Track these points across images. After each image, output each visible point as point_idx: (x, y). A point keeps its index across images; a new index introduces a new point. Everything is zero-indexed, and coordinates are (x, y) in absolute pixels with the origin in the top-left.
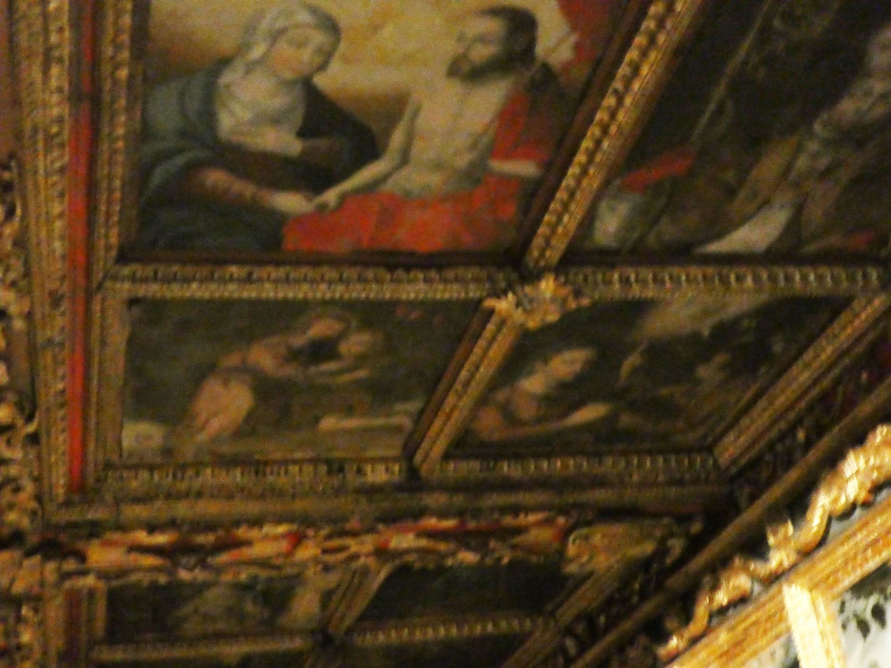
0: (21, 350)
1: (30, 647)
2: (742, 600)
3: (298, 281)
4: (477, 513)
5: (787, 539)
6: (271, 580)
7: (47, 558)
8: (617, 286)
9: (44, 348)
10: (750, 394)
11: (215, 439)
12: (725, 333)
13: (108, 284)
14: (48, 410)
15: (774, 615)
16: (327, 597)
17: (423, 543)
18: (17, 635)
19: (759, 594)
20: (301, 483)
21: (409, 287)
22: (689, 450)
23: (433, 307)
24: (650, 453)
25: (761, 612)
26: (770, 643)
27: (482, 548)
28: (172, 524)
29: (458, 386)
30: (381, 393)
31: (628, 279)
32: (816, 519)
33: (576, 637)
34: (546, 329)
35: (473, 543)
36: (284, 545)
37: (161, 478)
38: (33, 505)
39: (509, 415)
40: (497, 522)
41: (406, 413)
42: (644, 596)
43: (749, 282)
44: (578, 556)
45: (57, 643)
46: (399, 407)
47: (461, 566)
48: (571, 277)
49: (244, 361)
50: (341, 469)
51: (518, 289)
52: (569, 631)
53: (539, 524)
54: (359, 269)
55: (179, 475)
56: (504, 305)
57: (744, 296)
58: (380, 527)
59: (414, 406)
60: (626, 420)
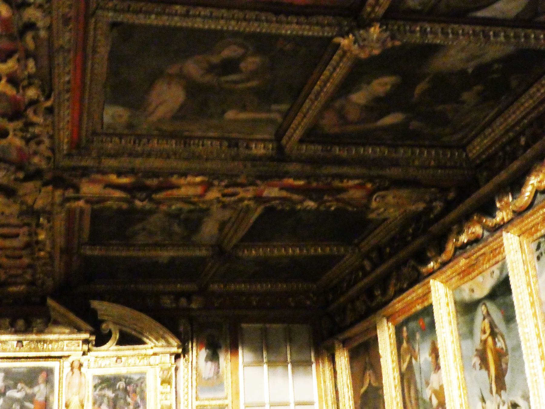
0: (43, 51)
1: (43, 243)
2: (476, 241)
3: (217, 18)
4: (317, 178)
5: (508, 204)
6: (191, 211)
7: (56, 187)
8: (418, 35)
9: (25, 110)
10: (492, 114)
11: (160, 121)
12: (483, 71)
13: (99, 12)
14: (59, 94)
15: (496, 249)
16: (223, 225)
17: (284, 194)
18: (36, 234)
19: (488, 237)
20: (212, 153)
21: (288, 26)
22: (449, 147)
23: (300, 41)
24: (426, 147)
25: (487, 248)
26: (490, 267)
27: (319, 200)
28: (132, 172)
29: (312, 96)
30: (265, 97)
31: (426, 29)
32: (528, 192)
33: (370, 259)
34: (372, 59)
35: (314, 196)
36: (199, 190)
37: (126, 143)
38: (48, 153)
39: (342, 116)
40: (330, 184)
41: (278, 111)
42: (415, 236)
43: (502, 38)
44: (377, 208)
45: (61, 241)
46: (274, 107)
47: (305, 210)
48: (390, 26)
49: (181, 69)
50: (237, 145)
51: (356, 32)
52: (367, 256)
53: (357, 187)
54: (257, 13)
55: (137, 142)
56: (345, 42)
57: (498, 46)
58: (259, 182)
59: (284, 107)
60: (415, 124)
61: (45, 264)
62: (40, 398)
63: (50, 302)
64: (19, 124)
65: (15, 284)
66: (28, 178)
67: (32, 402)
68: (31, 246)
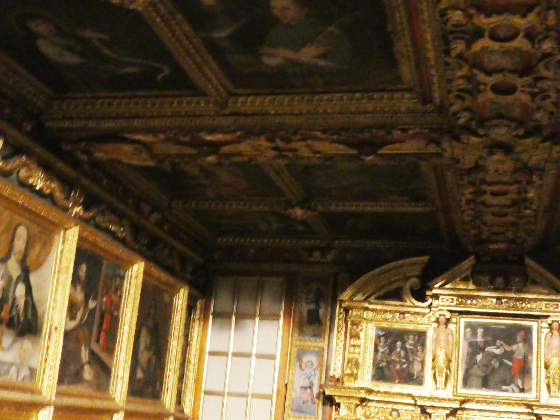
1: (531, 201)
9: (536, 65)
18: (526, 192)
45: (546, 200)
61: (529, 223)
62: (519, 356)
63: (529, 261)
64: (528, 79)
65: (496, 242)
66: (528, 134)
67: (511, 360)
68: (520, 203)
